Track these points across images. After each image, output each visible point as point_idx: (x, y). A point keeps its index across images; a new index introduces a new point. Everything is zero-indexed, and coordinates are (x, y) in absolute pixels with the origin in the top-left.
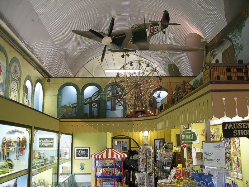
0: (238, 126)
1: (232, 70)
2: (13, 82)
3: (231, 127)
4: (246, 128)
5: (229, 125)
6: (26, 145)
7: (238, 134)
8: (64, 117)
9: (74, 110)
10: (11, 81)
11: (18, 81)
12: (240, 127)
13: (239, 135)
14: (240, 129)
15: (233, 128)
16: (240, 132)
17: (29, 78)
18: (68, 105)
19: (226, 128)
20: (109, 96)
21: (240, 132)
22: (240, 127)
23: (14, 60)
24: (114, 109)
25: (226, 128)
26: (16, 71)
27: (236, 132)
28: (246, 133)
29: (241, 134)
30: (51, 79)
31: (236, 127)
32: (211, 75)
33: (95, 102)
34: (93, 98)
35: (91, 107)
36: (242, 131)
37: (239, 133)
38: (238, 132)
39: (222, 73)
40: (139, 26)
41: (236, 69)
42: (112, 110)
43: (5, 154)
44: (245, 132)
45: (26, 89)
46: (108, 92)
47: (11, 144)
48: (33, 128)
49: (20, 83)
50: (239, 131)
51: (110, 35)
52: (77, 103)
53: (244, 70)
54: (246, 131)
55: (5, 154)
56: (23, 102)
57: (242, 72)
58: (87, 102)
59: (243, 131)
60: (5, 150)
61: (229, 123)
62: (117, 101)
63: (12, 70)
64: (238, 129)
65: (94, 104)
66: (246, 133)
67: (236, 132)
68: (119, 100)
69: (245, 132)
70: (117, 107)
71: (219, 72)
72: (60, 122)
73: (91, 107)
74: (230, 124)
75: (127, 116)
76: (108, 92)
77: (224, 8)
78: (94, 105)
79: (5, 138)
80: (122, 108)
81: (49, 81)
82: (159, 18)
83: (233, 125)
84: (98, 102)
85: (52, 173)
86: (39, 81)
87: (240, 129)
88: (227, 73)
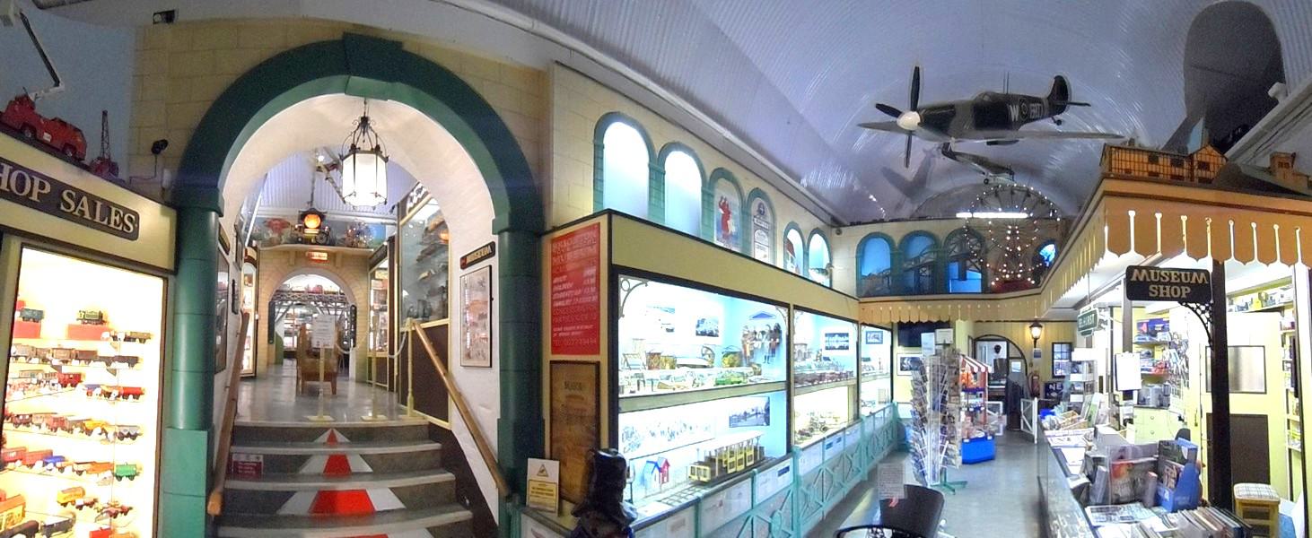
0: (1161, 276)
1: (1161, 160)
2: (759, 231)
3: (1145, 277)
4: (1178, 281)
5: (1140, 272)
6: (780, 338)
7: (1159, 294)
8: (868, 295)
9: (886, 282)
10: (753, 231)
11: (771, 232)
12: (1164, 278)
13: (1162, 295)
14: (1165, 284)
15: (1148, 280)
16: (1165, 289)
17: (793, 226)
18: (875, 273)
19: (1134, 279)
20: (953, 254)
21: (1165, 289)
22: (1164, 278)
23: (757, 193)
24: (963, 277)
25: (1134, 279)
26: (761, 213)
27: (1154, 288)
28: (1176, 293)
29: (1165, 294)
30: (843, 229)
31: (1156, 278)
32: (1113, 166)
33: (924, 265)
34: (922, 259)
35: (918, 275)
36: (1168, 287)
37: (1162, 291)
38: (1159, 290)
39: (1132, 160)
40: (994, 96)
41: (1169, 160)
42: (959, 279)
43: (748, 354)
44: (1175, 290)
45: (789, 246)
46: (952, 247)
47: (757, 337)
48: (792, 307)
49: (774, 234)
50: (1161, 287)
51: (914, 108)
52: (891, 269)
53: (1186, 165)
54: (1178, 288)
55: (748, 354)
56: (785, 266)
57: (1183, 168)
58: (910, 266)
59: (1181, 294)
60: (748, 346)
61: (1139, 268)
62: (968, 263)
63: (754, 209)
64: (1159, 283)
65: (924, 269)
66: (1176, 293)
67: (1154, 288)
68: (973, 261)
69: (1175, 290)
70: (970, 274)
71: (1126, 161)
72: (860, 303)
73: (918, 275)
74: (1144, 271)
75: (986, 289)
76: (952, 247)
77: (1183, 85)
78: (924, 272)
79: (746, 327)
80: (979, 275)
81: (839, 233)
82: (1043, 90)
83: (1149, 273)
84: (931, 266)
85: (43, 322)
86: (816, 231)
87: (1165, 284)
88: (1150, 166)
